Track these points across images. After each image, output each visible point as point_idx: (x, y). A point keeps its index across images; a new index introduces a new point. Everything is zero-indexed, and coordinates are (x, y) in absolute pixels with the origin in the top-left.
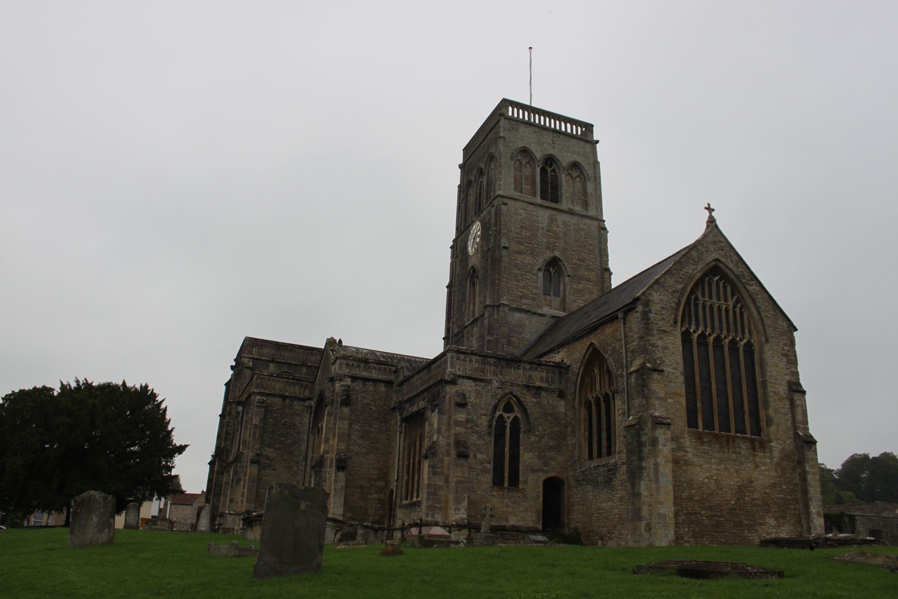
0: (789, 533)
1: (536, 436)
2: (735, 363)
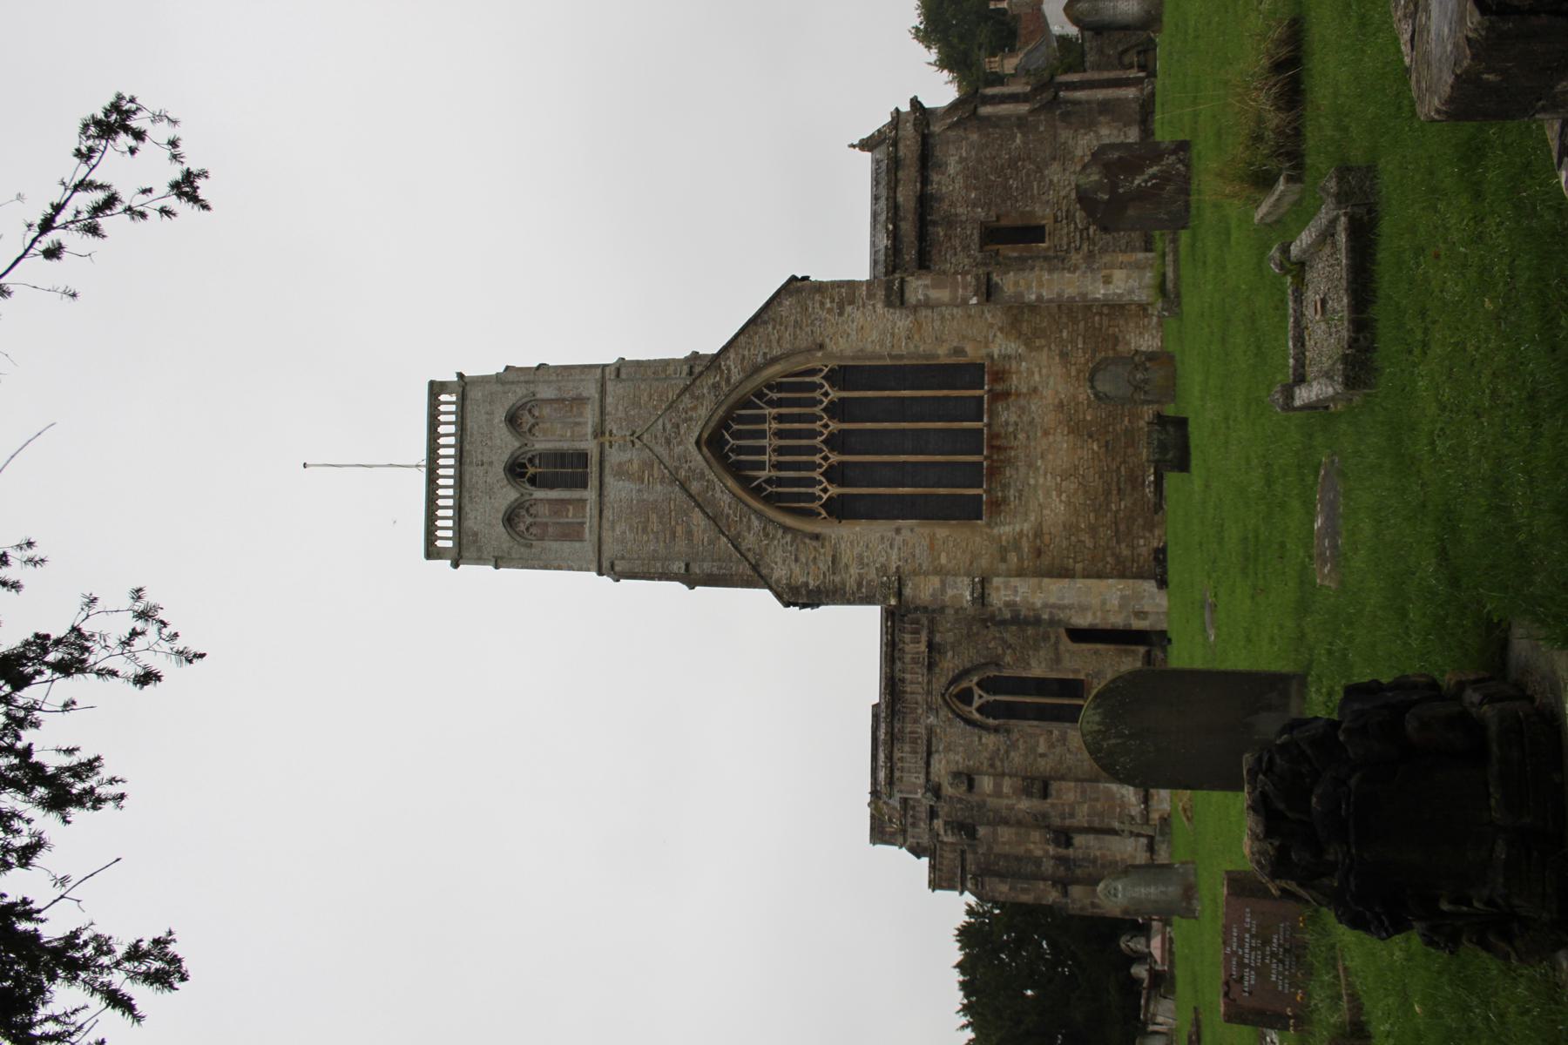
0: (1140, 333)
1: (1004, 653)
2: (876, 442)
